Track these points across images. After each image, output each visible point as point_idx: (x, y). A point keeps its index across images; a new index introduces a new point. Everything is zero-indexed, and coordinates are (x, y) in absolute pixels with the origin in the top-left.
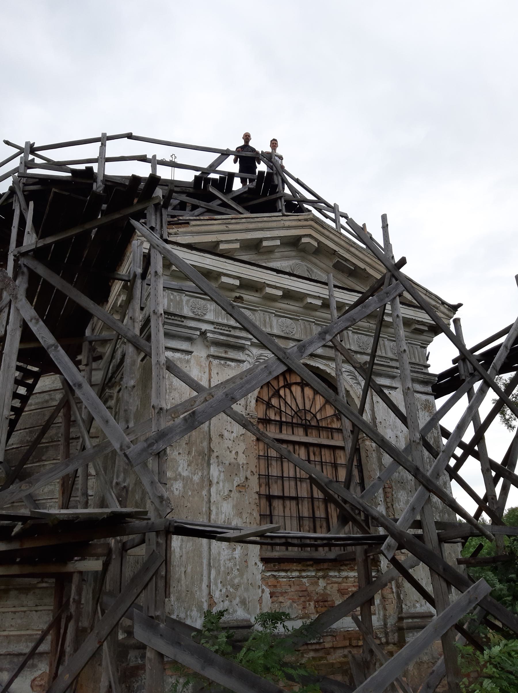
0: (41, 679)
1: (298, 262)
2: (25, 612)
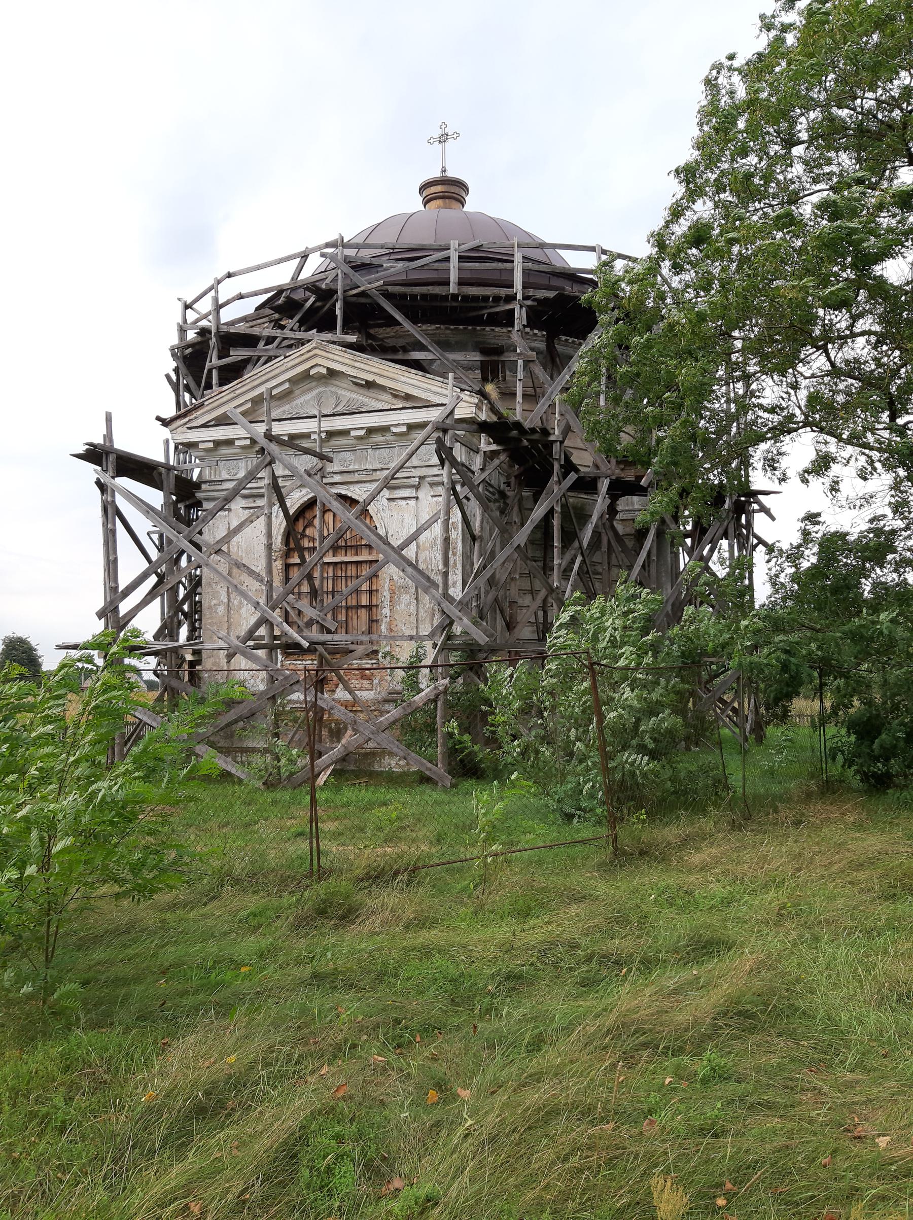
1: (321, 389)
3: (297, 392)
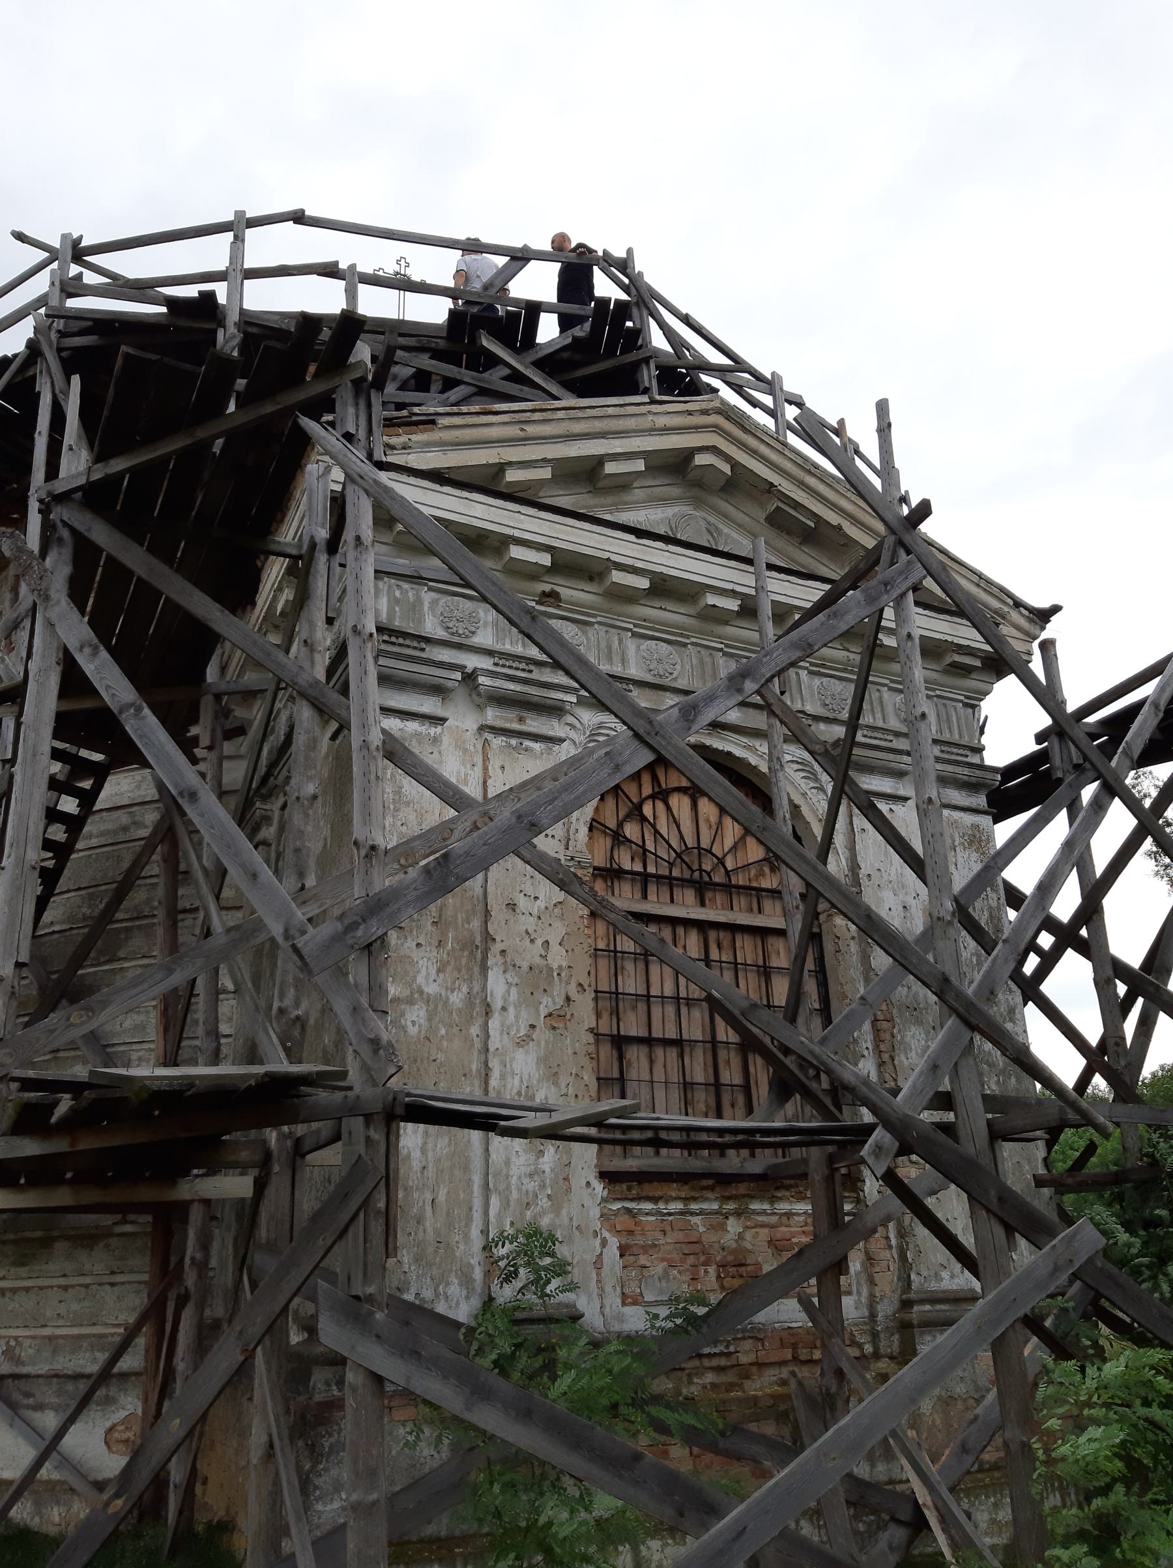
0: (127, 1428)
1: (686, 509)
2: (87, 1286)
3: (639, 494)
